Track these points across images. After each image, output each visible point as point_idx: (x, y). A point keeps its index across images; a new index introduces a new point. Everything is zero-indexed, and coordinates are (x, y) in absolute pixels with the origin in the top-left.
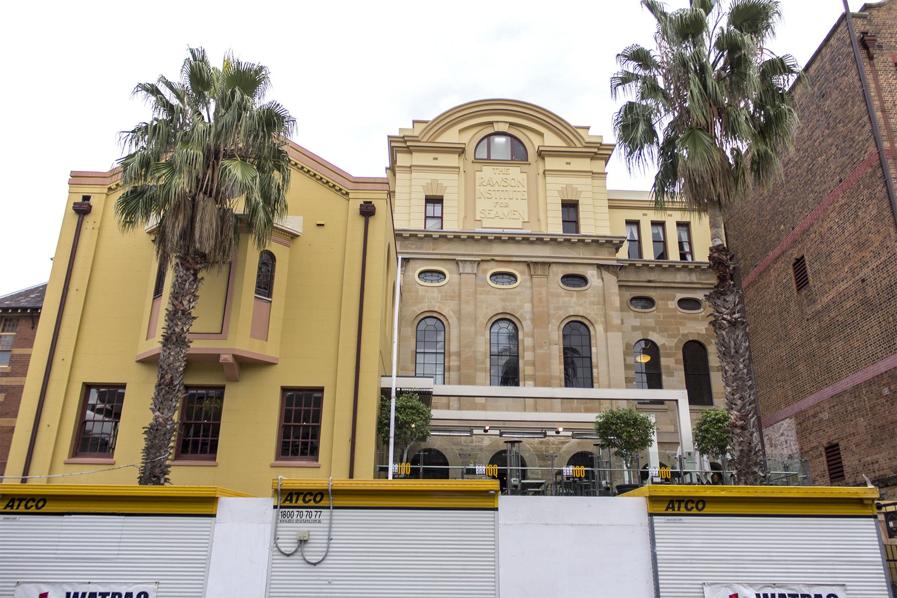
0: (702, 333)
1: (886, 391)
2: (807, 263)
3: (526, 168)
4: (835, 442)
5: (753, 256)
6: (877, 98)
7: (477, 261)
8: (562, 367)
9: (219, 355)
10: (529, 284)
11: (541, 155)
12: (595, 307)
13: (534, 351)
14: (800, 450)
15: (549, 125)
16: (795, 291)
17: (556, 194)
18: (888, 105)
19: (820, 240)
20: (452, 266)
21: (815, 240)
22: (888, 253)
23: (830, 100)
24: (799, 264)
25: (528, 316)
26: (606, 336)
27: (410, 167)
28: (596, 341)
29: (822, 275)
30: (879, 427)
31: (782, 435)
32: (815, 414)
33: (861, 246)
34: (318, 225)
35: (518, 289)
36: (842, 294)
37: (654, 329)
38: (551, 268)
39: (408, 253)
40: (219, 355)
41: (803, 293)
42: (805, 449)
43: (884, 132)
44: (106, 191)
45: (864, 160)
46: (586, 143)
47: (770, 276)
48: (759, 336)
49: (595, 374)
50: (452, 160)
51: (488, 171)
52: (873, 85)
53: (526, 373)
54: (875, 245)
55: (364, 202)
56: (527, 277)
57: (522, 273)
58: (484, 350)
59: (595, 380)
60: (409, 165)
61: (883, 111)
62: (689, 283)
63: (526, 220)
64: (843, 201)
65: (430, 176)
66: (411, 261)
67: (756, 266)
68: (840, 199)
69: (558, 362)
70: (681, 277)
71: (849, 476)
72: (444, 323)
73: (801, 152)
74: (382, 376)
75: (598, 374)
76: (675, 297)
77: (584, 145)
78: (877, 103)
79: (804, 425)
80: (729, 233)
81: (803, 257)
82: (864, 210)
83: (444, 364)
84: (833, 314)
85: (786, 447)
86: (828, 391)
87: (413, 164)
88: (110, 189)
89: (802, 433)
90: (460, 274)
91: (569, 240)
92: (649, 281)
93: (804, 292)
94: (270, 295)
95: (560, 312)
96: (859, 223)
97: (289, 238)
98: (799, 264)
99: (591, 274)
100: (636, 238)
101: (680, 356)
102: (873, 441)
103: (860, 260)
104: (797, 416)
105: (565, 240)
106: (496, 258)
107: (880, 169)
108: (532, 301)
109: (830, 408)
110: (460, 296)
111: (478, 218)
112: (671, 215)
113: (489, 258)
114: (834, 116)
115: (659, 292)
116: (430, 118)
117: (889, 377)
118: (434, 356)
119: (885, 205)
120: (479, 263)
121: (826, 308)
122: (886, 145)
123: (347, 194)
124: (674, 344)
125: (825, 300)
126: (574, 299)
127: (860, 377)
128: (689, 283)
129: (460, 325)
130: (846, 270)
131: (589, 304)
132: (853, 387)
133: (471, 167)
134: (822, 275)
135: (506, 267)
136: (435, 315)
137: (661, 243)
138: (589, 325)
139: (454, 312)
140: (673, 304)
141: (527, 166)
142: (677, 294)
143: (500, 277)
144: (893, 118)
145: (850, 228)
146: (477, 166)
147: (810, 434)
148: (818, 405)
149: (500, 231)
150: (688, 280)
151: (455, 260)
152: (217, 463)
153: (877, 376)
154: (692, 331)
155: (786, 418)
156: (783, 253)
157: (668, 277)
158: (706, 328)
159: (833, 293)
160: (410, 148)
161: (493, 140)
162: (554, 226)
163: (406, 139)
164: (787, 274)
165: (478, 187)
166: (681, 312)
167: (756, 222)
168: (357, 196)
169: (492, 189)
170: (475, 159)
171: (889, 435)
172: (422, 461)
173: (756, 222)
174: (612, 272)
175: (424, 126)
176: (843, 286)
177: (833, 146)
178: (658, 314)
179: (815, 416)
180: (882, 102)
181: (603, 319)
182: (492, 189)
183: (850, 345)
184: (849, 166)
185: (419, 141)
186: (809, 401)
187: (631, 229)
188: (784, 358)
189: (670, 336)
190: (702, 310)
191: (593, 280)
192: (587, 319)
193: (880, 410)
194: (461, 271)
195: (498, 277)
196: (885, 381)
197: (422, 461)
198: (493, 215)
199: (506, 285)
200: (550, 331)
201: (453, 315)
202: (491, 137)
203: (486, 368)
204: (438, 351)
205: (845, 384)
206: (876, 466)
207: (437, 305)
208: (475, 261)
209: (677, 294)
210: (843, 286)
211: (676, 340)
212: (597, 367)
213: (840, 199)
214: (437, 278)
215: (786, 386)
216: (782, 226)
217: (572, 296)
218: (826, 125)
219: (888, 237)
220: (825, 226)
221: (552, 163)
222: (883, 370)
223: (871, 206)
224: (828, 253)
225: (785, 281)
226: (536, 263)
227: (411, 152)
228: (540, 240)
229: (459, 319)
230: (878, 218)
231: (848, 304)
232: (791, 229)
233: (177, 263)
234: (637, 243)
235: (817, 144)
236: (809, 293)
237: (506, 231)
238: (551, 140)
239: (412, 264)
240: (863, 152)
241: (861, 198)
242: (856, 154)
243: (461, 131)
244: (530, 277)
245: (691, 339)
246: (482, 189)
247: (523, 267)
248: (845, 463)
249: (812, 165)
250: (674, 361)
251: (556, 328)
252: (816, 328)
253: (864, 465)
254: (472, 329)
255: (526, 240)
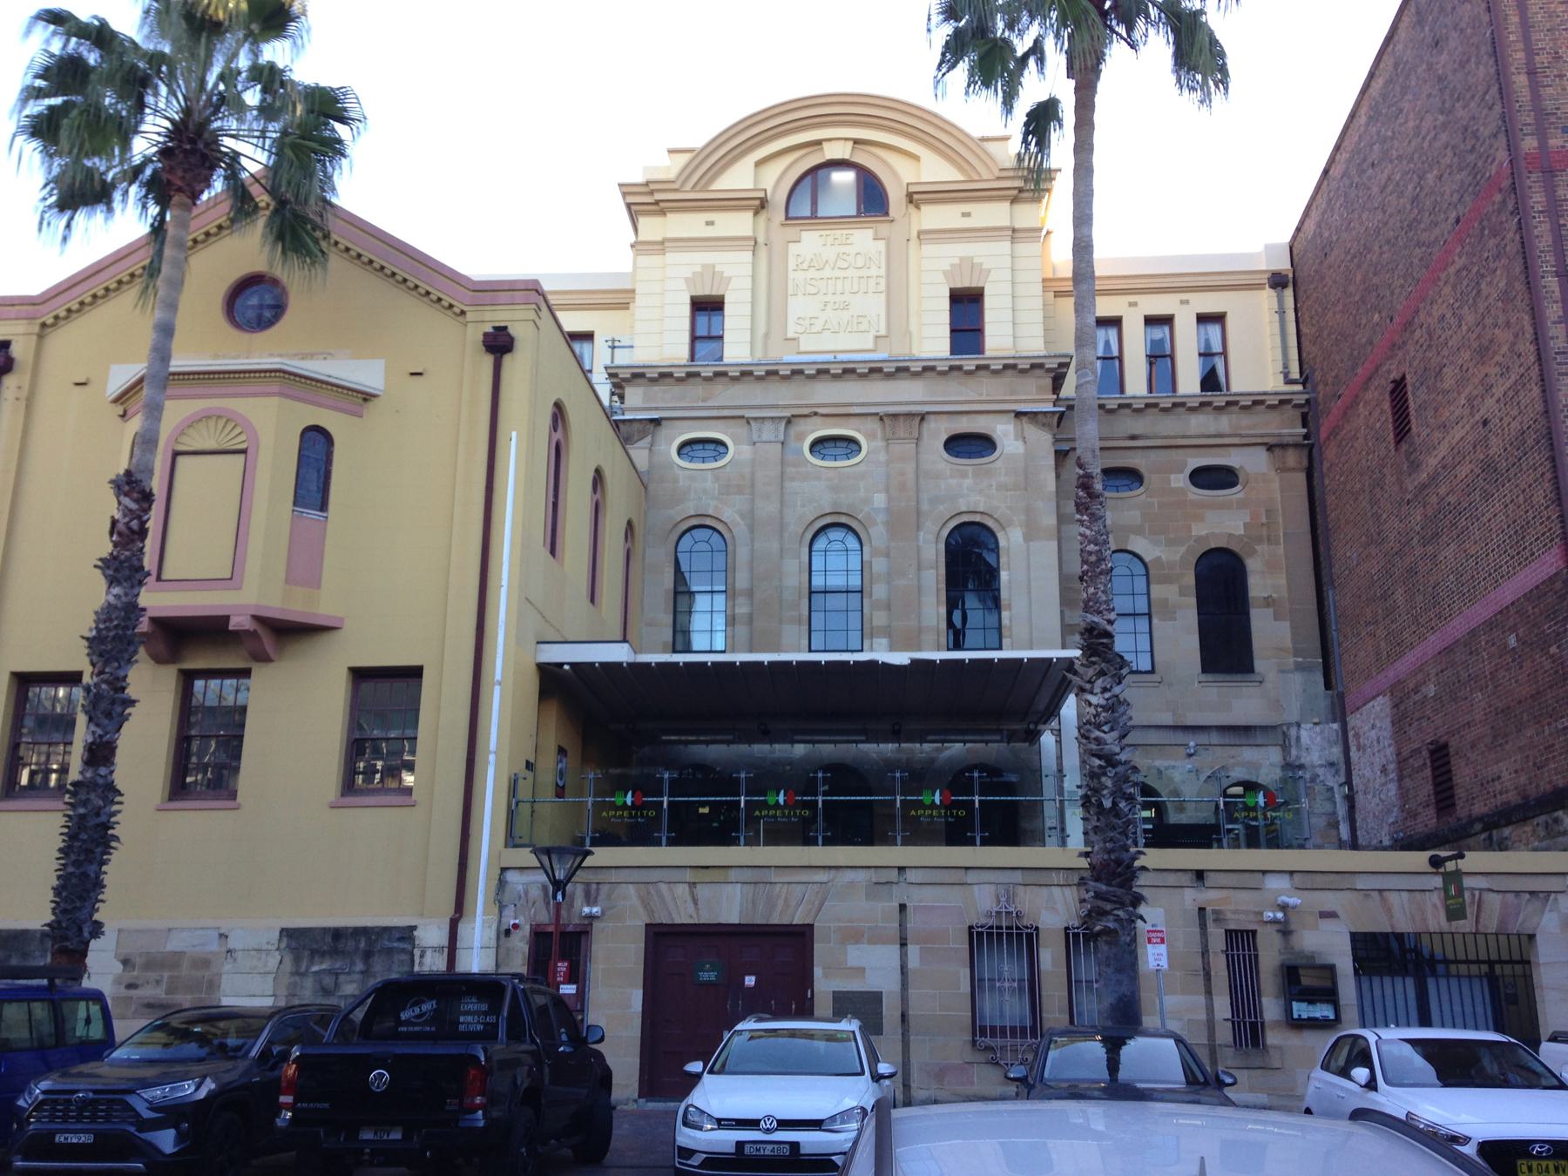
0: (1237, 533)
1: (1512, 641)
2: (1409, 388)
3: (884, 229)
4: (1442, 740)
5: (1336, 377)
6: (1520, 45)
7: (784, 418)
8: (943, 610)
9: (227, 618)
10: (882, 457)
11: (914, 198)
12: (1009, 493)
13: (888, 583)
14: (1397, 755)
15: (932, 140)
16: (1392, 446)
17: (941, 278)
18: (1542, 59)
19: (1428, 343)
20: (740, 429)
21: (1421, 342)
22: (1520, 367)
23: (1446, 52)
24: (1398, 389)
25: (881, 518)
26: (1028, 547)
27: (662, 243)
28: (1009, 557)
29: (1430, 413)
30: (1502, 711)
31: (1373, 727)
32: (1416, 687)
33: (1483, 352)
34: (412, 374)
35: (862, 467)
36: (1456, 451)
37: (1138, 531)
38: (925, 425)
39: (657, 409)
40: (227, 618)
41: (1403, 450)
42: (1405, 754)
43: (1528, 116)
44: (36, 329)
45: (1490, 176)
46: (1001, 170)
47: (1359, 416)
48: (1342, 536)
49: (1005, 621)
50: (740, 223)
51: (811, 242)
52: (1515, 19)
53: (874, 624)
54: (1502, 352)
55: (494, 328)
56: (880, 444)
57: (870, 436)
58: (797, 584)
59: (1004, 632)
60: (659, 238)
61: (1532, 73)
62: (1215, 436)
63: (883, 332)
64: (1461, 263)
65: (699, 259)
66: (663, 423)
67: (1339, 397)
68: (1456, 258)
69: (934, 599)
70: (1200, 424)
71: (1462, 804)
72: (726, 536)
73: (1405, 162)
74: (538, 643)
75: (1011, 620)
76: (1185, 465)
77: (997, 174)
78: (1520, 55)
79: (1402, 708)
80: (1304, 330)
81: (1403, 378)
82: (1488, 279)
83: (862, 610)
84: (1442, 490)
85: (1379, 751)
86: (1434, 642)
87: (670, 235)
88: (44, 325)
89: (1400, 721)
90: (754, 443)
91: (959, 368)
92: (1133, 438)
93: (1404, 447)
94: (323, 506)
95: (941, 507)
96: (1482, 306)
97: (360, 401)
98: (1398, 389)
99: (1004, 432)
100: (1115, 353)
101: (1190, 580)
102: (1495, 737)
103: (1482, 383)
104: (1392, 689)
105: (952, 368)
106: (820, 411)
107: (1513, 196)
108: (887, 490)
109: (1437, 674)
110: (753, 485)
111: (791, 334)
112: (1187, 302)
113: (806, 411)
114: (1451, 86)
115: (1153, 455)
116: (699, 143)
117: (1517, 612)
118: (709, 596)
119: (1518, 268)
120: (789, 421)
121: (1433, 478)
122: (1529, 144)
123: (463, 313)
124: (1178, 558)
125: (1432, 462)
126: (968, 482)
127: (1480, 612)
128: (1215, 436)
129: (752, 540)
130: (1463, 402)
131: (997, 489)
132: (1468, 633)
133: (779, 234)
134: (1430, 413)
135: (841, 426)
136: (708, 522)
137: (1160, 358)
138: (995, 530)
139: (742, 516)
140: (1180, 481)
141: (886, 225)
142: (1189, 460)
143: (830, 449)
144: (1550, 86)
145: (1470, 318)
146: (791, 232)
147: (1410, 725)
148: (1420, 669)
149: (830, 357)
150: (1212, 430)
151: (743, 417)
152: (239, 805)
153: (1501, 612)
154: (1217, 531)
155: (1378, 695)
156: (1377, 369)
157: (1168, 426)
158: (1245, 524)
159: (1443, 450)
160: (662, 204)
161: (828, 178)
162: (933, 340)
163: (652, 187)
164: (1382, 412)
165: (791, 275)
166: (1197, 494)
167: (1340, 307)
168: (478, 317)
169: (817, 275)
170: (787, 218)
171: (1516, 727)
172: (977, 787)
173: (1340, 307)
174: (1044, 425)
175: (687, 157)
176: (1457, 433)
177: (1450, 148)
178: (1149, 499)
179: (1416, 691)
180: (1530, 52)
181: (1023, 517)
182: (817, 275)
183: (1465, 551)
184: (1471, 189)
185: (676, 190)
186: (1403, 666)
187: (1107, 334)
188: (1375, 577)
189: (1172, 543)
190: (1239, 487)
191: (1006, 442)
192: (991, 516)
193: (1504, 676)
194: (755, 438)
195: (826, 445)
196: (1511, 622)
197: (977, 787)
198: (818, 326)
199: (842, 459)
200: (921, 543)
201: (742, 523)
202: (821, 173)
203: (800, 615)
204: (716, 588)
205: (1457, 627)
206: (1497, 785)
207: (713, 503)
208: (781, 418)
209: (1189, 460)
210: (1457, 433)
211: (1183, 549)
212: (1009, 607)
213: (1456, 258)
214: (714, 454)
215: (1378, 633)
216: (1377, 316)
217: (964, 476)
218: (1440, 105)
219: (1520, 334)
220: (1434, 313)
221: (935, 216)
222: (1509, 599)
223: (1498, 272)
224: (1438, 368)
225: (1378, 425)
226: (895, 416)
227: (663, 213)
228: (902, 371)
229: (752, 529)
230: (1506, 297)
231: (1463, 471)
232: (1388, 321)
233: (1399, 349)
234: (1113, 361)
235: (1426, 145)
236: (1411, 450)
237: (840, 357)
238: (934, 170)
239: (664, 432)
240: (1490, 160)
241: (1486, 255)
242: (1480, 164)
243: (759, 164)
244: (884, 444)
245: (1213, 546)
246: (800, 275)
247: (873, 425)
248: (1457, 779)
249: (1418, 189)
250: (1177, 589)
251: (932, 537)
252: (1419, 518)
253: (1482, 785)
254: (775, 546)
255: (875, 371)
